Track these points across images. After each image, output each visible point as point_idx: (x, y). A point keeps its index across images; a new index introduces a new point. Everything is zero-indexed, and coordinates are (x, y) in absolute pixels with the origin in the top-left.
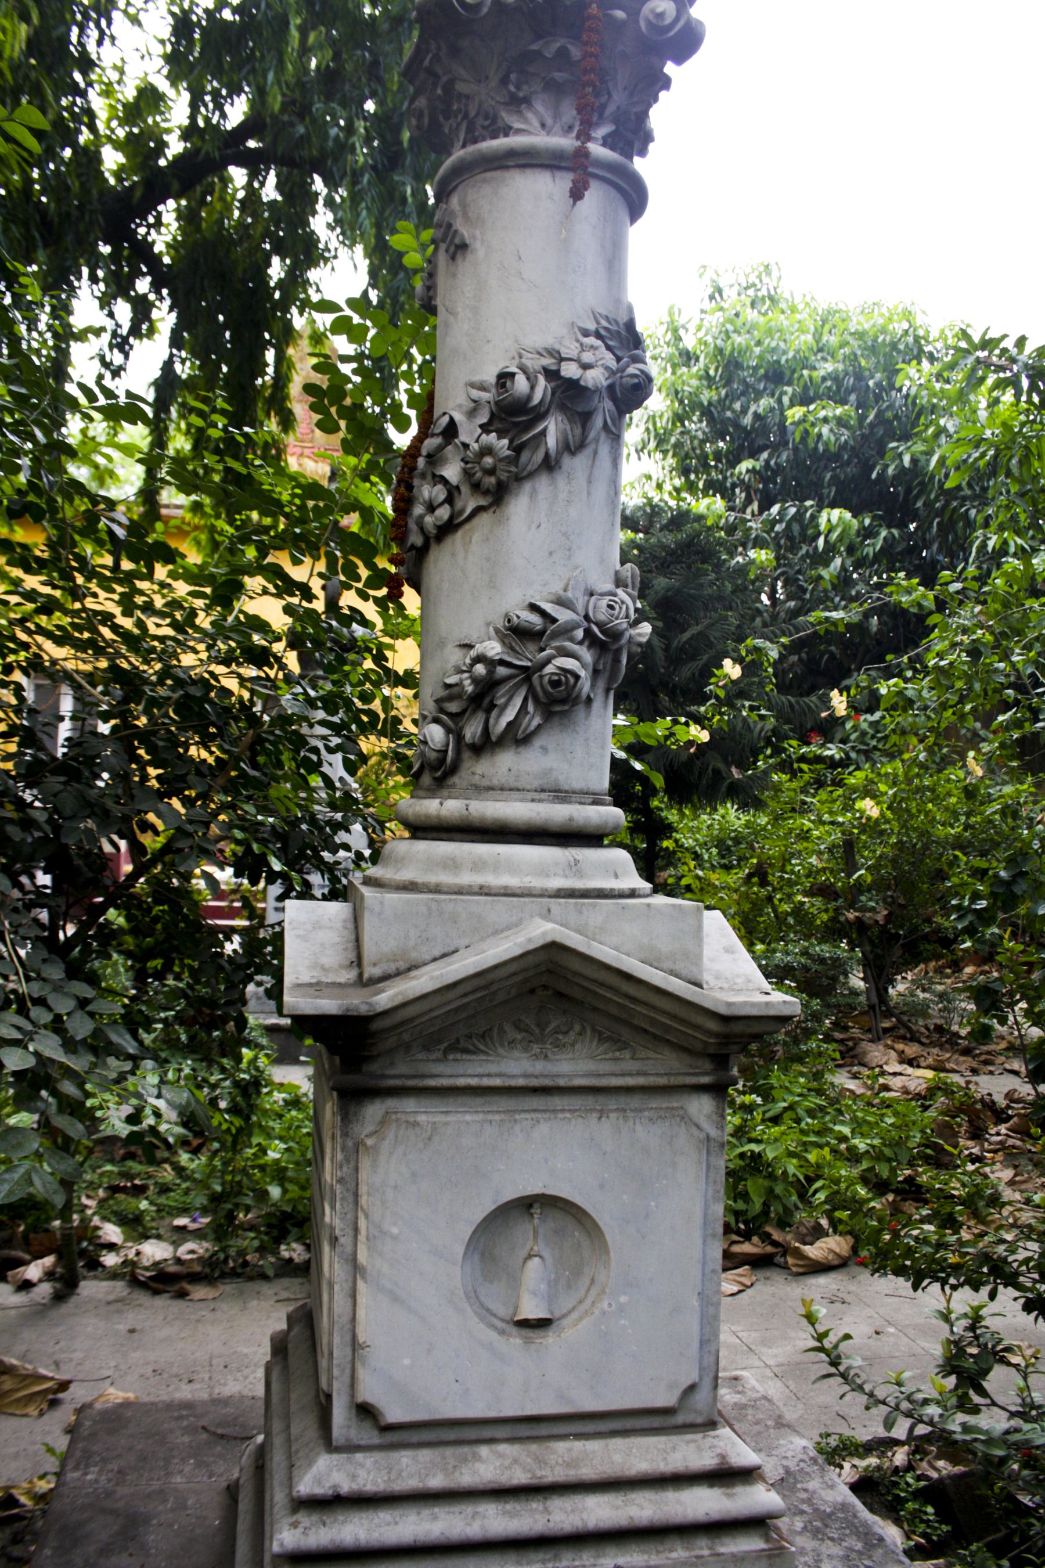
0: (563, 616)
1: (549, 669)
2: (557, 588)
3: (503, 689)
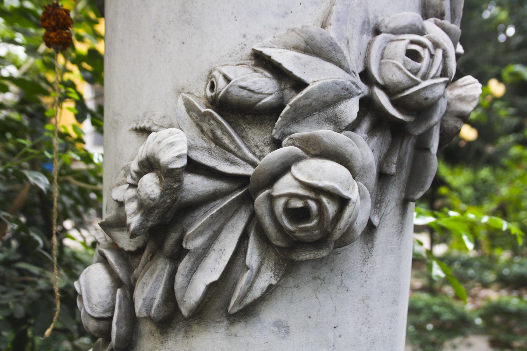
0: (318, 75)
1: (285, 185)
2: (308, 20)
3: (202, 219)
